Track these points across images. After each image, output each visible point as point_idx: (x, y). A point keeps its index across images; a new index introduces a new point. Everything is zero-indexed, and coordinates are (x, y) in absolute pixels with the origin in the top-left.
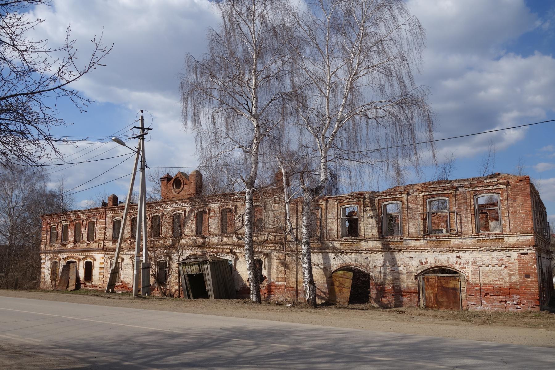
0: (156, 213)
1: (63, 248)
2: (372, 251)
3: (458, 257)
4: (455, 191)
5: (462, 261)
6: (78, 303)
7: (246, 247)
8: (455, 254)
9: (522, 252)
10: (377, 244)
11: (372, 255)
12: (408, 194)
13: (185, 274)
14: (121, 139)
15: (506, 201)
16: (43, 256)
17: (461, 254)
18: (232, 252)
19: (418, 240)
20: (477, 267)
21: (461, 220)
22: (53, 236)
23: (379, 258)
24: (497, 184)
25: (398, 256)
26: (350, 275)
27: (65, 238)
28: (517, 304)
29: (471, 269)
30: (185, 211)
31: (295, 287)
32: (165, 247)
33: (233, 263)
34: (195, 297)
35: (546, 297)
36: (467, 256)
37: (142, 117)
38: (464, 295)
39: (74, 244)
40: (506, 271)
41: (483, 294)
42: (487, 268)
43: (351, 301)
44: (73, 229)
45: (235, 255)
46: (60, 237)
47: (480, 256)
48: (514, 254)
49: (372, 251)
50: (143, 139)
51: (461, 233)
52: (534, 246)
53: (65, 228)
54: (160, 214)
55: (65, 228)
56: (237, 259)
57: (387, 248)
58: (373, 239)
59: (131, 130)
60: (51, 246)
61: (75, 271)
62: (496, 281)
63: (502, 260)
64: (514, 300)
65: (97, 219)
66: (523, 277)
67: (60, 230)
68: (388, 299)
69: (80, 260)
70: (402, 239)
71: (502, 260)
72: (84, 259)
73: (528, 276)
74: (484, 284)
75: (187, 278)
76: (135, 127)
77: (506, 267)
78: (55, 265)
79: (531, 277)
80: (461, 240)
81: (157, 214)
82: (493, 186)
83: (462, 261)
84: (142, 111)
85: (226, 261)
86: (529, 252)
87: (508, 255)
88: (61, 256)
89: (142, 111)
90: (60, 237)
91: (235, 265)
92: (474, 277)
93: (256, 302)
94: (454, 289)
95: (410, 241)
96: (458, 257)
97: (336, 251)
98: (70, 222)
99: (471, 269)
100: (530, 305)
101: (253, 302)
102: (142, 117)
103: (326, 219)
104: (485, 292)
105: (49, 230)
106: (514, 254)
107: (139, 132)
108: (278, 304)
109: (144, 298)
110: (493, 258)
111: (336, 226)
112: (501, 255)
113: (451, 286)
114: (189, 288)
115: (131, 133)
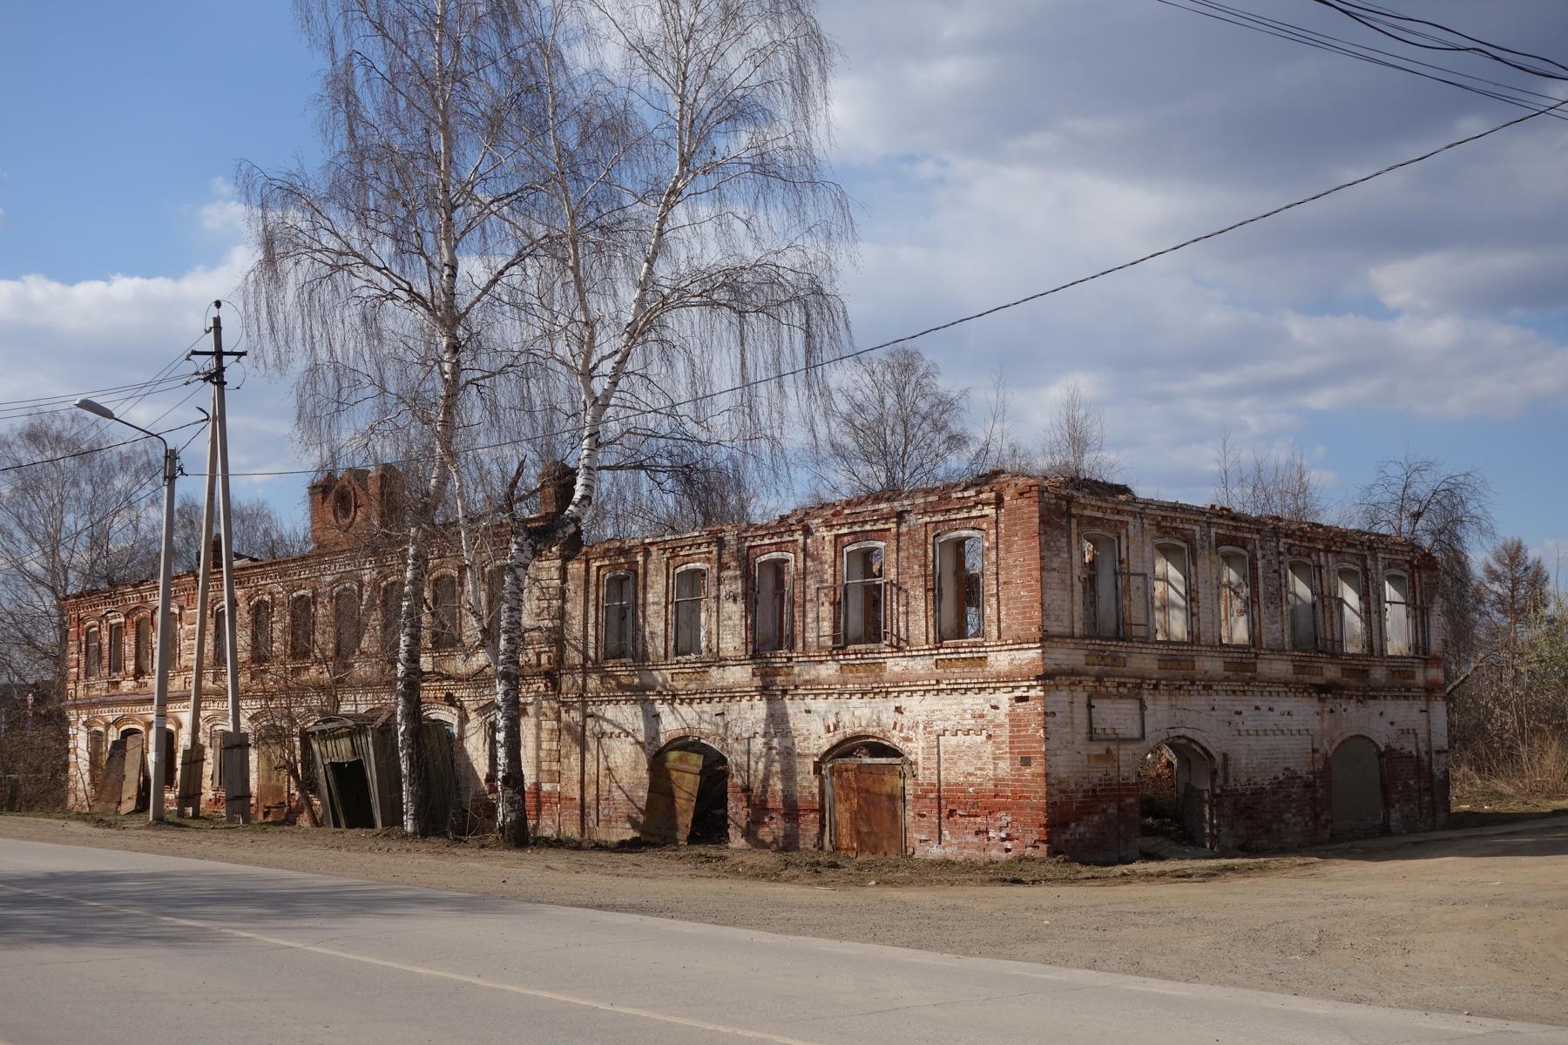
0: (300, 587)
1: (113, 692)
2: (730, 694)
3: (898, 710)
4: (898, 524)
5: (904, 720)
6: (17, 838)
7: (400, 686)
8: (892, 703)
9: (1018, 693)
10: (739, 675)
11: (734, 707)
12: (807, 532)
13: (327, 761)
14: (97, 400)
15: (994, 553)
16: (72, 715)
17: (903, 701)
18: (450, 700)
19: (821, 662)
20: (933, 737)
21: (907, 604)
22: (92, 655)
23: (754, 712)
24: (977, 504)
25: (792, 707)
26: (696, 761)
27: (116, 665)
28: (1009, 838)
29: (922, 744)
30: (361, 585)
31: (577, 796)
32: (321, 688)
33: (455, 730)
34: (351, 826)
35: (1219, 825)
36: (917, 706)
37: (217, 321)
38: (910, 815)
39: (136, 679)
40: (989, 747)
41: (945, 812)
42: (954, 740)
43: (693, 839)
44: (133, 637)
45: (461, 708)
46: (105, 662)
47: (940, 706)
48: (1004, 699)
49: (730, 694)
50: (221, 384)
51: (907, 642)
52: (1038, 678)
53: (116, 632)
54: (307, 592)
55: (116, 632)
56: (464, 719)
57: (770, 688)
58: (739, 662)
59: (188, 359)
60: (87, 687)
61: (138, 757)
62: (970, 774)
63: (982, 716)
64: (1001, 829)
65: (181, 608)
66: (1018, 762)
67: (106, 640)
68: (773, 829)
69: (108, 725)
70: (790, 659)
71: (982, 716)
72: (116, 723)
73: (1026, 762)
74: (948, 784)
75: (330, 773)
76: (194, 353)
77: (989, 737)
78: (96, 739)
79: (1034, 764)
80: (904, 662)
81: (302, 592)
82: (970, 508)
83: (904, 720)
84: (218, 304)
85: (440, 723)
86: (1032, 693)
87: (994, 702)
88: (110, 715)
89: (218, 304)
90: (105, 662)
91: (462, 738)
92: (927, 765)
93: (415, 833)
94: (891, 797)
95: (805, 667)
96: (898, 710)
97: (673, 697)
98: (126, 616)
99: (922, 744)
100: (1030, 841)
101: (406, 836)
102: (217, 321)
103: (644, 605)
104: (948, 805)
105: (83, 638)
106: (1004, 699)
107: (209, 363)
108: (558, 843)
109: (178, 825)
110: (965, 711)
111: (662, 625)
112: (973, 702)
113: (887, 789)
114: (336, 800)
115: (190, 367)
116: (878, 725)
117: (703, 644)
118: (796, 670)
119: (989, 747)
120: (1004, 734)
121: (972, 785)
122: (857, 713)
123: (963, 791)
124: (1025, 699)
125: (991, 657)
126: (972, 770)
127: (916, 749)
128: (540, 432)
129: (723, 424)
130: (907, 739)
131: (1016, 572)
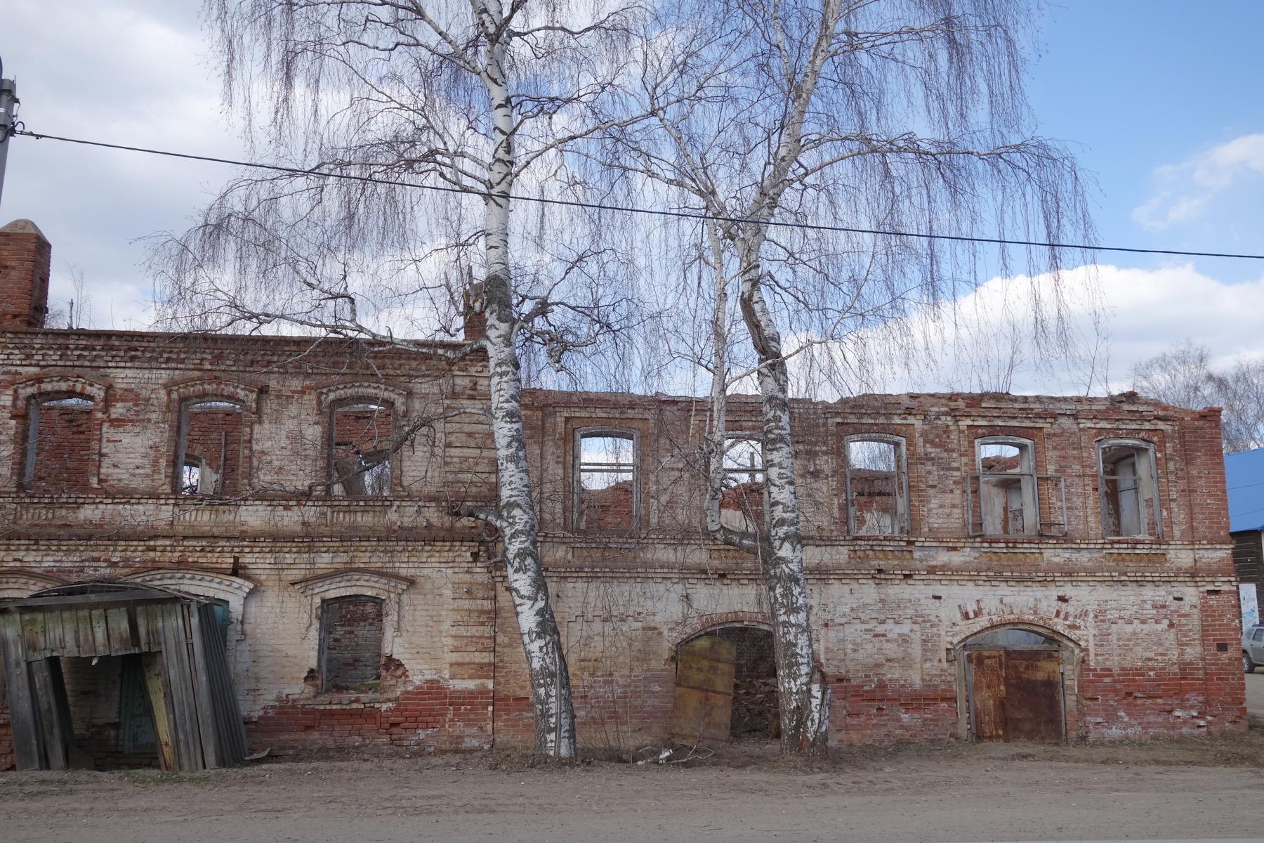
3: (1062, 599)
8: (1054, 592)
17: (1068, 591)
36: (1084, 596)
40: (1172, 635)
47: (1114, 596)
63: (1163, 607)
71: (1163, 607)
77: (1171, 625)
79: (1230, 649)
83: (1070, 608)
87: (1177, 595)
96: (1062, 599)
99: (1093, 631)
106: (1191, 594)
110: (1144, 601)
113: (1040, 676)
116: (1035, 613)
117: (195, 621)
118: (917, 554)
119: (1172, 635)
120: (1195, 620)
121: (1152, 669)
122: (1006, 600)
123: (1143, 675)
124: (1216, 592)
125: (1171, 554)
126: (1152, 655)
127: (1088, 633)
128: (652, 477)
129: (613, 744)
130: (1073, 627)
131: (1202, 482)
